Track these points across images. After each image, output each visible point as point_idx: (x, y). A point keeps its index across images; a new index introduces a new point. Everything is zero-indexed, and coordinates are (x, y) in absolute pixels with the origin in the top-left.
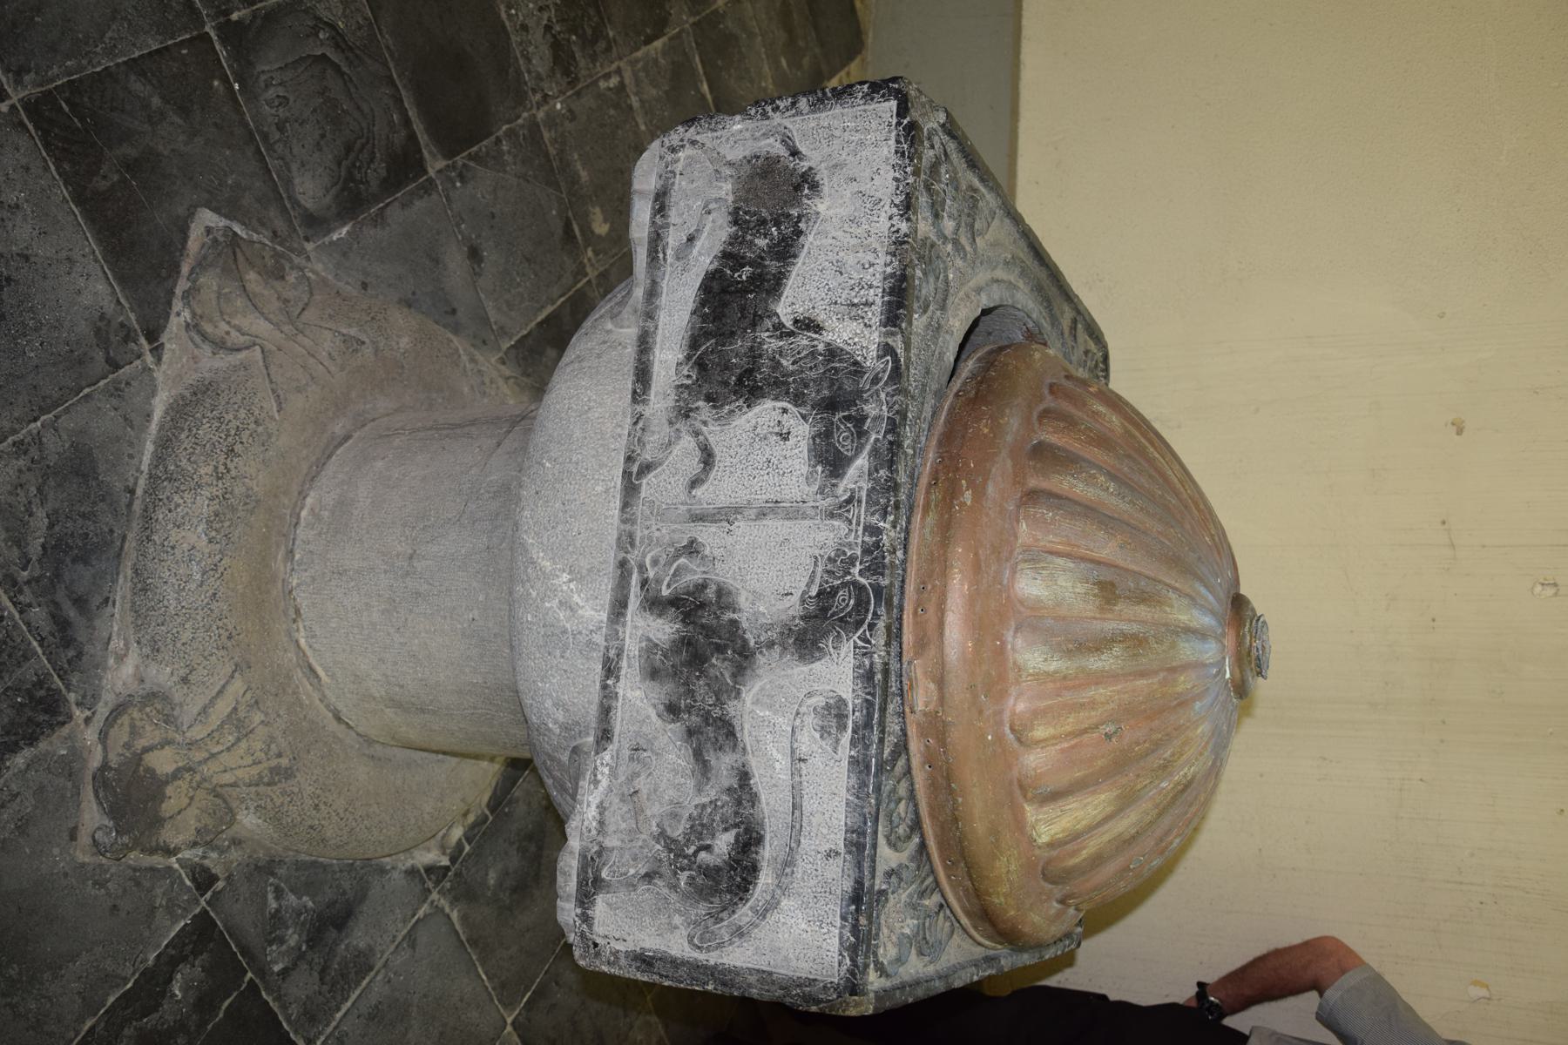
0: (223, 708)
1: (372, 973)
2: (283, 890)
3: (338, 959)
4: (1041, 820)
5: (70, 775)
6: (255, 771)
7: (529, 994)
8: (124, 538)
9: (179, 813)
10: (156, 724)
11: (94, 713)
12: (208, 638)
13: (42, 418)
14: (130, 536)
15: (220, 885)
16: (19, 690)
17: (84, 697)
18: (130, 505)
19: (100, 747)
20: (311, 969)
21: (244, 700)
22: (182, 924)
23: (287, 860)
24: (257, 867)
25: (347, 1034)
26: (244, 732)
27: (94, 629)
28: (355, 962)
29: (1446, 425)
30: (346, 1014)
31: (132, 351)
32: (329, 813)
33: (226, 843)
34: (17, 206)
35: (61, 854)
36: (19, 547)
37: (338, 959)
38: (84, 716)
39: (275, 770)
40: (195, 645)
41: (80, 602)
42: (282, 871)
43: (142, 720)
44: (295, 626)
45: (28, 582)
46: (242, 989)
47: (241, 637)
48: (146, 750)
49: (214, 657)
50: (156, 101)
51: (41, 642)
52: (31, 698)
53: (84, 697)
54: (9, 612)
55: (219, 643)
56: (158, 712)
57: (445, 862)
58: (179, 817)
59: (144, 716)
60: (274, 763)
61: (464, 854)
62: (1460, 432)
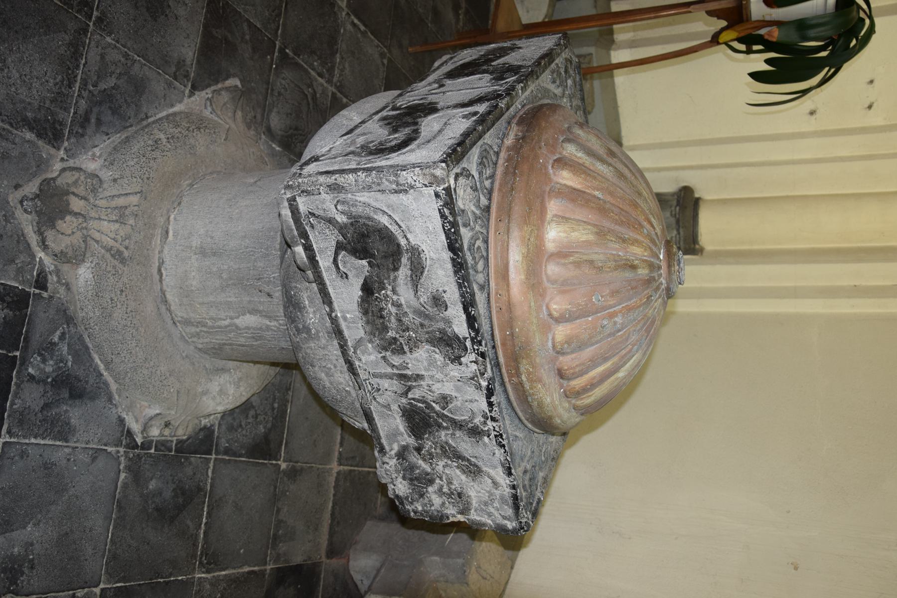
0: (121, 202)
1: (65, 444)
2: (65, 339)
3: (57, 410)
4: (554, 220)
5: (38, 166)
6: (111, 243)
7: (123, 584)
8: (131, 126)
9: (62, 234)
10: (87, 189)
11: (67, 160)
12: (139, 170)
13: (141, 59)
14: (134, 128)
15: (45, 295)
16: (53, 115)
17: (70, 150)
18: (143, 120)
19: (58, 173)
20: (43, 396)
21: (132, 208)
22: (17, 285)
23: (79, 328)
24: (65, 311)
25: (28, 456)
26: (122, 221)
27: (95, 136)
28: (63, 425)
29: (788, 564)
30: (37, 444)
31: (184, 82)
32: (124, 302)
33: (64, 281)
34: (186, 5)
35: (6, 186)
36: (98, 77)
37: (57, 410)
38: (62, 156)
39: (119, 253)
40: (132, 169)
41: (99, 122)
42: (73, 330)
43: (82, 182)
44: (173, 210)
45: (90, 91)
46: (10, 354)
47: (152, 184)
48: (73, 193)
49: (136, 179)
50: (247, 37)
51: (75, 113)
52: (54, 123)
53: (70, 150)
54: (75, 90)
55: (142, 176)
56: (92, 185)
57: (139, 440)
58: (60, 235)
59: (85, 182)
60: (122, 249)
61: (149, 451)
62: (796, 568)
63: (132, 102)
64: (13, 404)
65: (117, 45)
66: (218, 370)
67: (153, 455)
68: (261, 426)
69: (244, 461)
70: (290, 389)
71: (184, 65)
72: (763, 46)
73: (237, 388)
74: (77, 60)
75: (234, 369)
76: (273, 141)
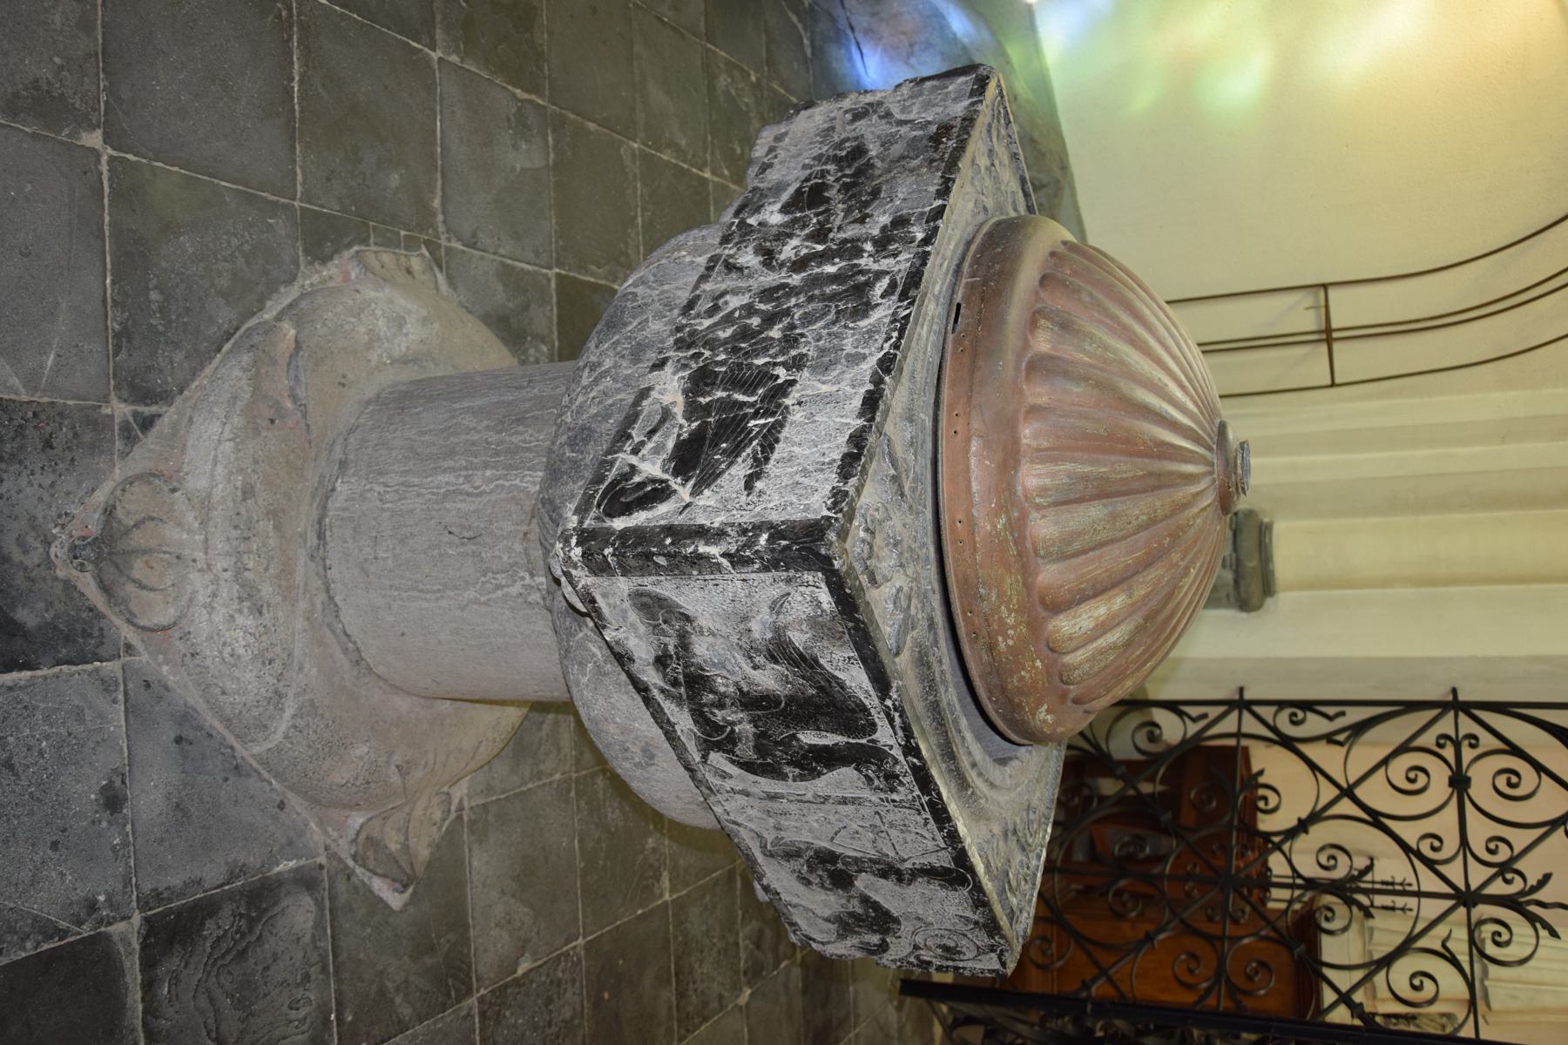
7: (411, 42)
50: (398, 1000)
64: (552, 310)
66: (414, 361)
67: (401, 226)
68: (190, 250)
70: (117, 336)
72: (1363, 1021)
73: (371, 330)
75: (385, 364)
76: (297, 870)
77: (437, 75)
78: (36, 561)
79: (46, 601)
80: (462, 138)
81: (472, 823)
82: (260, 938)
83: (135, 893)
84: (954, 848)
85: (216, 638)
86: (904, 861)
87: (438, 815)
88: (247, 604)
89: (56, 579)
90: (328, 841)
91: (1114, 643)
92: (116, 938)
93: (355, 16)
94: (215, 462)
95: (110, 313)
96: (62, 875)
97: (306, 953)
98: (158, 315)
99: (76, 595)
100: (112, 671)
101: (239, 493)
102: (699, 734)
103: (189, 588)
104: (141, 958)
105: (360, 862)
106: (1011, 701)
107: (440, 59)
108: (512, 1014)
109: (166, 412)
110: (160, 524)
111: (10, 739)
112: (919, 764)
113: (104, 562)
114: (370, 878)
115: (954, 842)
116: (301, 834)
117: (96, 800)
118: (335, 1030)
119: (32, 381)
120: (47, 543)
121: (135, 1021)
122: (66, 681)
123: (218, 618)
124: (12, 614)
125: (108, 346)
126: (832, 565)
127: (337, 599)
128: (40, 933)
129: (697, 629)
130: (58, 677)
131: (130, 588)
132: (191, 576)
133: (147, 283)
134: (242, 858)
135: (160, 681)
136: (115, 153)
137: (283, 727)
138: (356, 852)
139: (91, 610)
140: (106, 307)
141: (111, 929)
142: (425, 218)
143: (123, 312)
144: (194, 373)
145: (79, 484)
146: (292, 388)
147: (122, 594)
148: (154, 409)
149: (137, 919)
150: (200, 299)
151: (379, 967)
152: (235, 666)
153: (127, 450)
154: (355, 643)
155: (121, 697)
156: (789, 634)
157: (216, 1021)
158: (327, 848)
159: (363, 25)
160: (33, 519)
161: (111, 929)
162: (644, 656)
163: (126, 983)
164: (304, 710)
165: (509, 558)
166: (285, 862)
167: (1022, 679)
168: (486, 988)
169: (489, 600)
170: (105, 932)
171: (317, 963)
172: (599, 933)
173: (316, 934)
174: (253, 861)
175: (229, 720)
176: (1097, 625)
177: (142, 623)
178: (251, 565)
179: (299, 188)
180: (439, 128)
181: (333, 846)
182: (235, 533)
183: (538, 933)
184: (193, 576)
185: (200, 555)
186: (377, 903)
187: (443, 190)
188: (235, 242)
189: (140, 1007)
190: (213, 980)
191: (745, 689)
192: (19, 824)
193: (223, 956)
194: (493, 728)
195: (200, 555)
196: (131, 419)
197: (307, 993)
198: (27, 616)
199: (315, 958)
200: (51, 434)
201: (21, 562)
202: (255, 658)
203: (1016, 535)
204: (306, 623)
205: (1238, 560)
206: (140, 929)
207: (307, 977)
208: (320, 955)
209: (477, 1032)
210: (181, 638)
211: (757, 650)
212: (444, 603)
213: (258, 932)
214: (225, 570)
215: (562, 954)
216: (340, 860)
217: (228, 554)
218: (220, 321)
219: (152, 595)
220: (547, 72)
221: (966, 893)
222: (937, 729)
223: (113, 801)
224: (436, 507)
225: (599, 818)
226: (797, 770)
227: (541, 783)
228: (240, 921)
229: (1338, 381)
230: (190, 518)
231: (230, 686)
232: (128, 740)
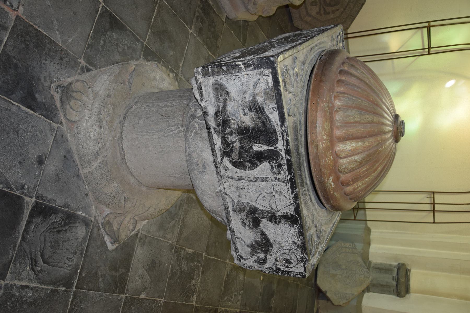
50: (101, 280)
63: (164, 218)
65: (168, 241)
69: (128, 27)
71: (141, 244)
74: (181, 229)
76: (84, 217)
77: (190, 36)
78: (47, 85)
79: (45, 97)
80: (192, 54)
81: (141, 239)
82: (66, 230)
83: (36, 192)
84: (296, 203)
85: (86, 130)
86: (278, 211)
87: (131, 228)
88: (98, 123)
89: (50, 93)
90: (96, 215)
91: (357, 159)
92: (25, 201)
93: (173, 11)
94: (103, 85)
95: (89, 39)
96: (18, 172)
97: (78, 245)
98: (101, 47)
99: (53, 100)
100: (55, 126)
101: (106, 95)
102: (222, 149)
103: (84, 114)
104: (30, 212)
105: (103, 227)
106: (321, 171)
107: (191, 33)
108: (134, 310)
109: (94, 70)
110: (82, 94)
111: (21, 126)
112: (289, 159)
113: (64, 93)
114: (105, 235)
115: (296, 200)
116: (90, 207)
117: (36, 158)
118: (78, 276)
119: (64, 42)
120: (52, 83)
121: (21, 231)
122: (42, 121)
123: (89, 124)
124: (35, 94)
125: (86, 46)
126: (274, 65)
127: (123, 136)
128: (6, 184)
129: (230, 98)
130: (40, 118)
131: (68, 107)
132: (86, 110)
133: (101, 38)
134: (70, 203)
135: (66, 137)
136: (104, 5)
137: (95, 165)
138: (103, 222)
139: (56, 106)
140: (89, 37)
141: (25, 197)
142: (177, 67)
143: (92, 41)
144: (105, 66)
145: (65, 73)
146: (129, 79)
147: (65, 107)
148: (91, 68)
149: (33, 200)
150: (113, 50)
151: (98, 265)
152: (89, 140)
153: (81, 73)
154: (124, 152)
155: (54, 135)
156: (257, 98)
157: (44, 247)
158: (95, 217)
159: (174, 14)
160: (50, 74)
161: (25, 197)
162: (212, 113)
163: (23, 217)
164: (103, 163)
165: (177, 122)
166: (82, 213)
167: (326, 161)
168: (129, 295)
169: (167, 135)
170: (23, 197)
171: (80, 250)
172: (170, 301)
173: (83, 241)
174: (73, 205)
175: (81, 158)
176: (352, 149)
177: (67, 117)
178: (103, 114)
179: (147, 40)
180: (186, 48)
181: (97, 217)
182: (101, 104)
183: (150, 288)
184: (86, 111)
185: (90, 106)
186: (104, 244)
187: (183, 63)
188: (126, 42)
189: (24, 227)
190: (47, 234)
191: (240, 125)
192: (13, 150)
193: (54, 228)
194: (156, 205)
195: (90, 106)
196: (85, 67)
197: (74, 258)
198: (39, 97)
199: (80, 248)
200: (63, 57)
201: (43, 83)
202: (95, 140)
203: (330, 111)
204: (112, 139)
205: (398, 278)
206: (33, 203)
207: (75, 253)
208: (82, 248)
209: (121, 308)
210: (76, 128)
211: (247, 107)
212: (154, 137)
213: (66, 228)
214: (95, 112)
215: (156, 300)
216: (98, 223)
217: (97, 108)
218: (116, 58)
219: (73, 112)
220: (218, 52)
221: (296, 228)
222: (297, 155)
223: (41, 161)
224: (160, 109)
225: (180, 264)
226: (250, 164)
227: (165, 240)
228: (62, 221)
229: (435, 222)
230: (91, 96)
231: (85, 146)
232: (51, 147)
